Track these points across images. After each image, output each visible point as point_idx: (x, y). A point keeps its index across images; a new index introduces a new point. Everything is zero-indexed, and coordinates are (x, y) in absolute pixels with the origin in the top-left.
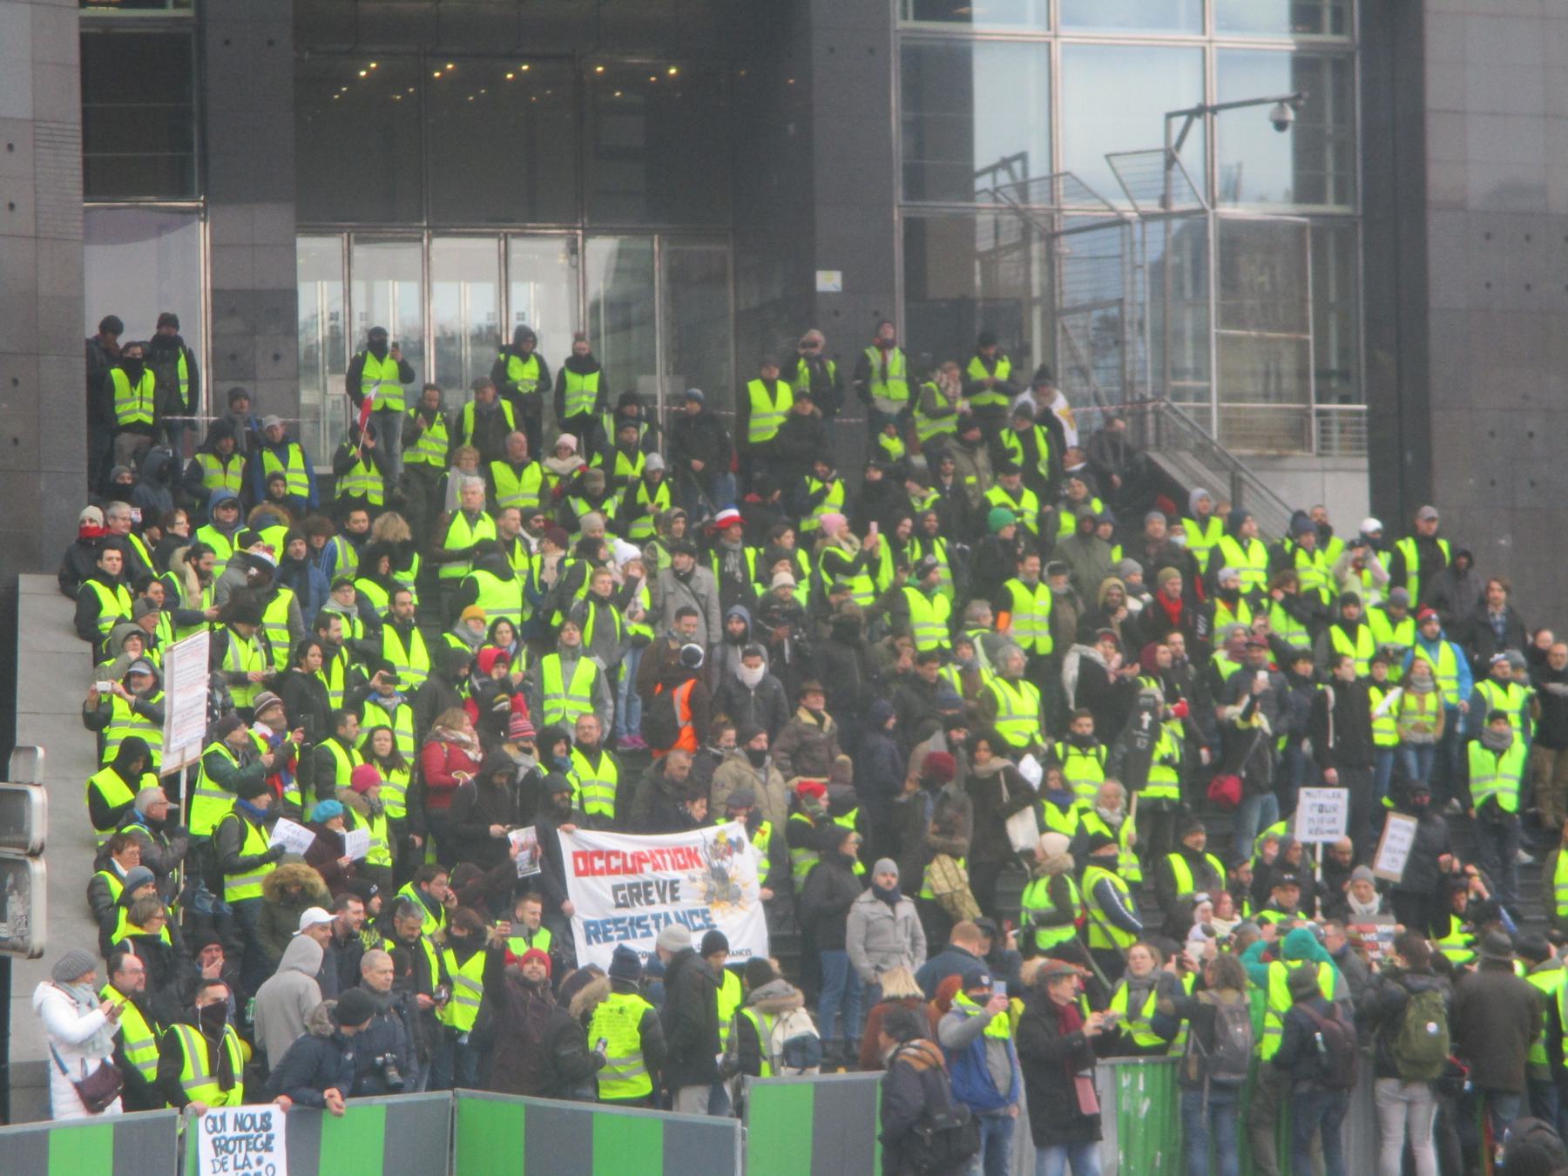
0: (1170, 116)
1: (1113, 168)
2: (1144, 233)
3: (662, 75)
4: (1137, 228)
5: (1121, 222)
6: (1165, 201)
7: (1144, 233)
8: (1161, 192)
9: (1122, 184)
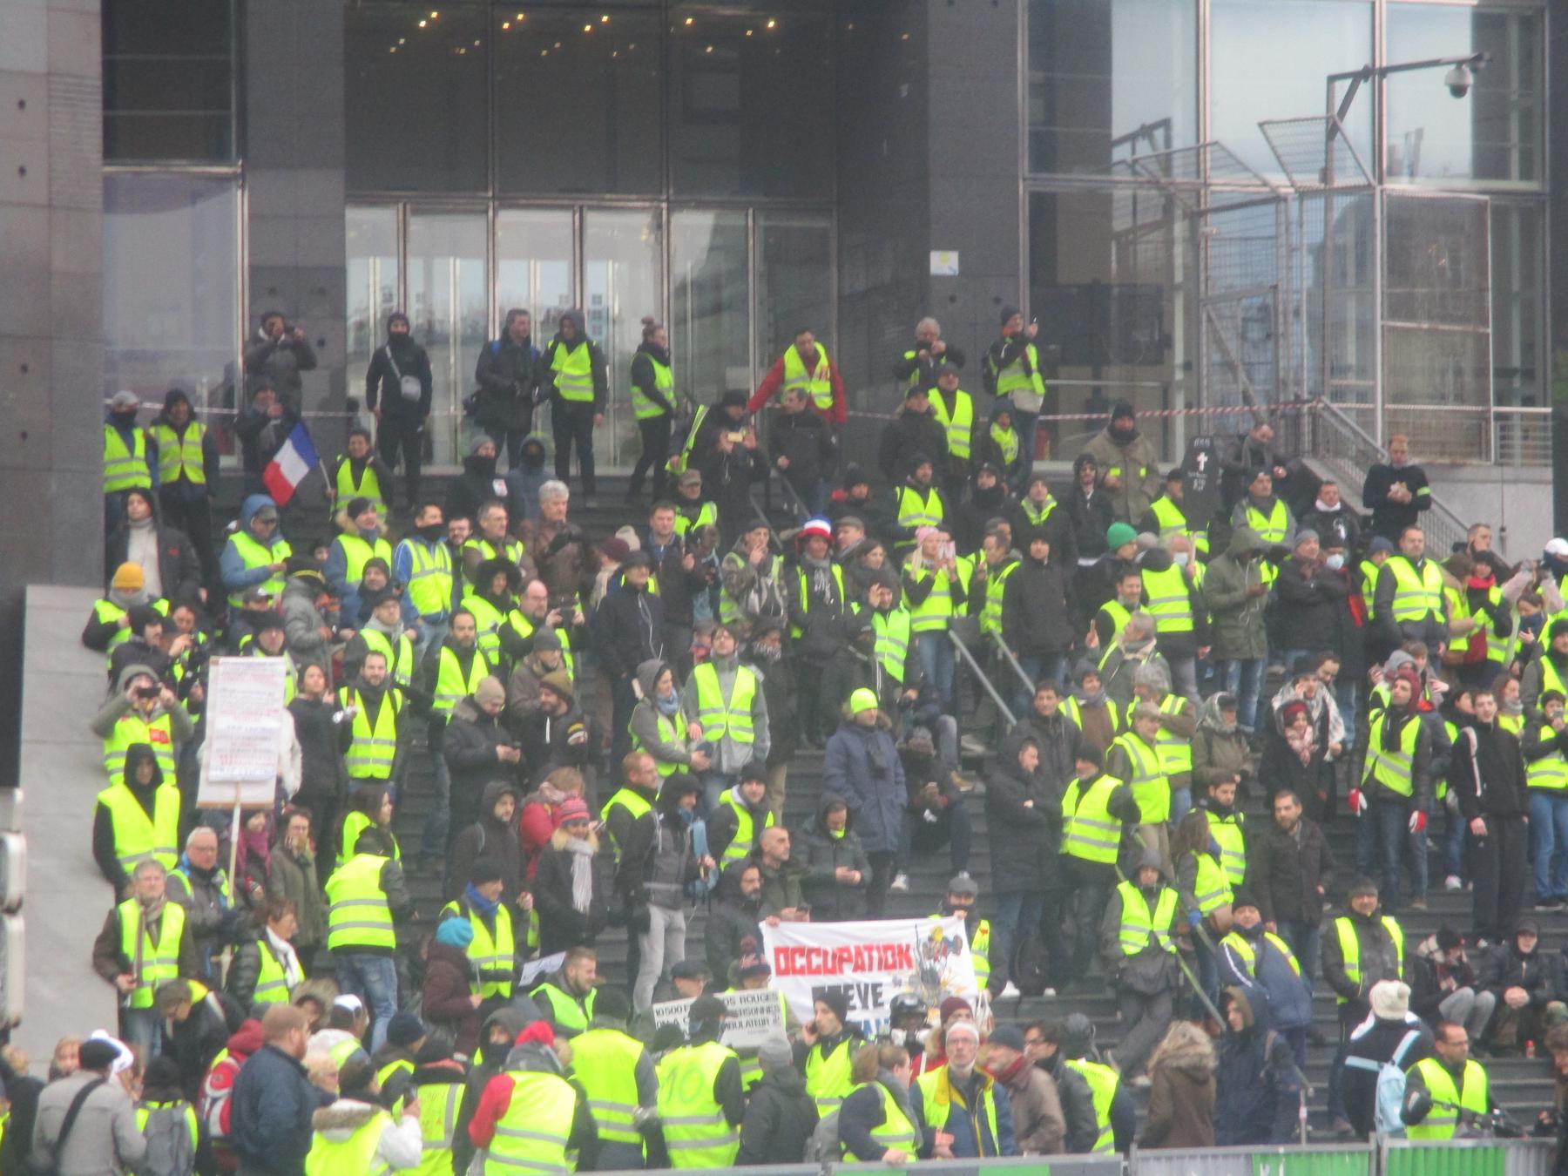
0: (1332, 79)
1: (1267, 138)
2: (1301, 211)
3: (760, 29)
4: (1294, 206)
5: (1277, 199)
6: (1326, 175)
7: (1301, 211)
8: (1323, 164)
9: (1278, 157)
